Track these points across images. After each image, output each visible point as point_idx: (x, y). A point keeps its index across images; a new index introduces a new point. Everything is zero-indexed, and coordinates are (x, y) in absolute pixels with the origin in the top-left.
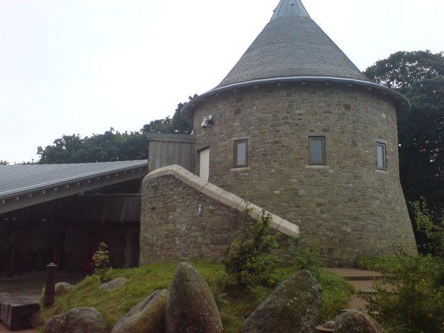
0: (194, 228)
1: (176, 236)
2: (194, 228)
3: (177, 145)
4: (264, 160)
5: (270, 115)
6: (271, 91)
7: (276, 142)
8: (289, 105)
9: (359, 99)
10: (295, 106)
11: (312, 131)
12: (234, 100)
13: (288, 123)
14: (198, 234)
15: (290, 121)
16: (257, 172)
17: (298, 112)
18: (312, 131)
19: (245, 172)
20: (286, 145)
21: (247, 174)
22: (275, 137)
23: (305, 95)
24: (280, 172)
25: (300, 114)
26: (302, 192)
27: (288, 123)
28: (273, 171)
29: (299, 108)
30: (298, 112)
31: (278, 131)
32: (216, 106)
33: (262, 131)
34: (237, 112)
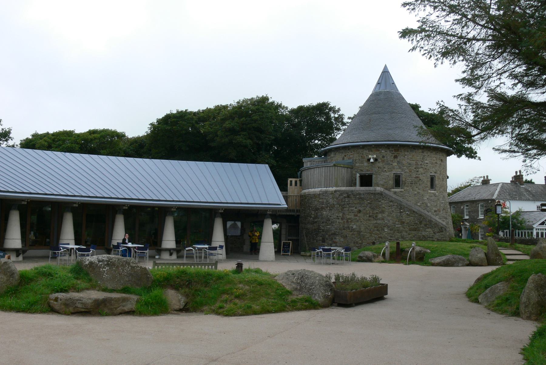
0: (397, 223)
1: (385, 227)
2: (397, 223)
3: (346, 169)
4: (411, 186)
5: (414, 162)
6: (415, 149)
7: (417, 177)
8: (423, 158)
9: (409, 151)
10: (425, 158)
11: (431, 173)
12: (393, 150)
13: (422, 168)
14: (399, 226)
15: (423, 166)
16: (408, 192)
17: (426, 162)
18: (431, 173)
19: (401, 192)
20: (422, 179)
21: (402, 193)
22: (416, 174)
23: (429, 153)
24: (418, 193)
25: (427, 163)
26: (429, 205)
27: (422, 168)
28: (416, 193)
29: (426, 160)
30: (426, 162)
31: (418, 171)
32: (379, 150)
33: (410, 170)
34: (395, 157)
